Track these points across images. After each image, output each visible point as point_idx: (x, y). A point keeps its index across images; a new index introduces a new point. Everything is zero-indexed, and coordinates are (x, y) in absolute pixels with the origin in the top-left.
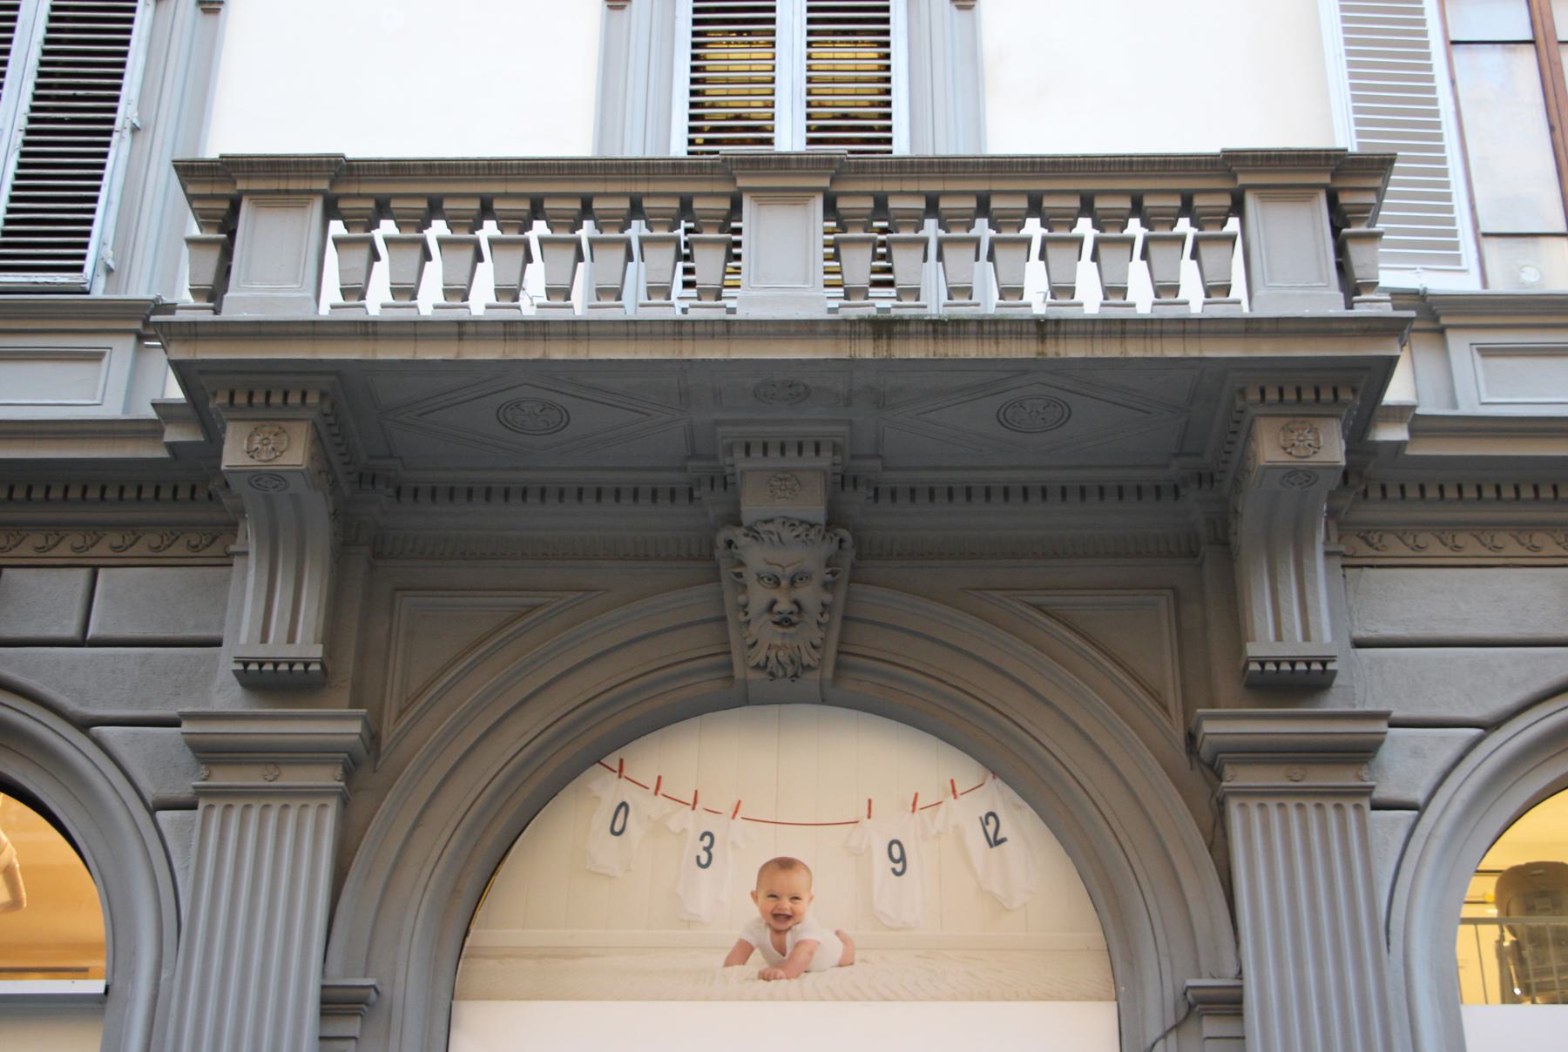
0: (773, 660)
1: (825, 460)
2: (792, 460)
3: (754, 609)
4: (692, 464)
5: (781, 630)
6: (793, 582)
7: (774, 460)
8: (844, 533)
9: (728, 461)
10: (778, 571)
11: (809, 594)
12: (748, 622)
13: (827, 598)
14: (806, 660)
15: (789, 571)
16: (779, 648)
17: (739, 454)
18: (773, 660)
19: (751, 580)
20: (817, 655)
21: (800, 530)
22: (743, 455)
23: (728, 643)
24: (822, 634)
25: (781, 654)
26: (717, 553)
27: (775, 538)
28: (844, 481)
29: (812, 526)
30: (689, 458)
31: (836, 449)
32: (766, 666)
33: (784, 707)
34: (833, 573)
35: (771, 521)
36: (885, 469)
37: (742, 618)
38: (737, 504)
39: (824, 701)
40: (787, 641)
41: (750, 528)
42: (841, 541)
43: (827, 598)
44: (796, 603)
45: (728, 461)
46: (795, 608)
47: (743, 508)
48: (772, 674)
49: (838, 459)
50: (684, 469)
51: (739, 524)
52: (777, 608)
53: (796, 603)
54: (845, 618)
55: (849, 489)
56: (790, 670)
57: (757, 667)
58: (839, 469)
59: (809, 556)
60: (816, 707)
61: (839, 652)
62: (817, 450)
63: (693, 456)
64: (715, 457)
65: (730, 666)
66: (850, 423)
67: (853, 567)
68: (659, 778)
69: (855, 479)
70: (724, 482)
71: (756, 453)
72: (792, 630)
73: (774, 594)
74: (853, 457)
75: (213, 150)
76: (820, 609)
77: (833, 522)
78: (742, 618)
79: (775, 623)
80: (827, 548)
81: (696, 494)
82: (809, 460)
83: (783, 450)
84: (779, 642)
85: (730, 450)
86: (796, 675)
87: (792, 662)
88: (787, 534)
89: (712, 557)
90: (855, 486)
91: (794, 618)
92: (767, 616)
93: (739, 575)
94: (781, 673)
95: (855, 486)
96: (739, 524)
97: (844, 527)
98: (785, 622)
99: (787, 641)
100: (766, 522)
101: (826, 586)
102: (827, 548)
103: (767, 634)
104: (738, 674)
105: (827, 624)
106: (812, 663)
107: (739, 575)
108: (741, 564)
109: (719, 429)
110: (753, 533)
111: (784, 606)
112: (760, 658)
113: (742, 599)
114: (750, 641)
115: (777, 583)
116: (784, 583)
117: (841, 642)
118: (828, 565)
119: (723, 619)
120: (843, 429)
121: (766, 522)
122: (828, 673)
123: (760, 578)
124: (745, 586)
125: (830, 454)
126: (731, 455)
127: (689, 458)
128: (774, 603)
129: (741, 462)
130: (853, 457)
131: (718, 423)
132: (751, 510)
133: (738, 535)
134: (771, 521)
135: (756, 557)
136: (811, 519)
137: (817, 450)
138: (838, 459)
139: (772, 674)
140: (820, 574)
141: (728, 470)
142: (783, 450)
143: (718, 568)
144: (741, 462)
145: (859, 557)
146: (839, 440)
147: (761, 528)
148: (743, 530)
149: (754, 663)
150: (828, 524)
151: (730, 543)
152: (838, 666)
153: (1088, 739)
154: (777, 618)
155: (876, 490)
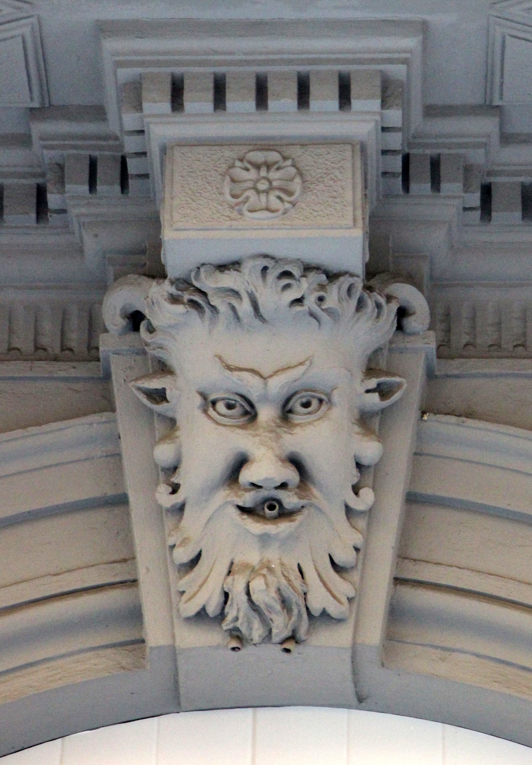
0: (238, 596)
1: (363, 120)
2: (283, 119)
3: (192, 479)
4: (39, 128)
5: (256, 527)
6: (286, 413)
7: (241, 120)
8: (407, 293)
9: (130, 120)
10: (252, 386)
11: (328, 441)
12: (181, 508)
13: (370, 450)
14: (319, 600)
15: (277, 386)
16: (254, 571)
17: (157, 104)
18: (238, 596)
19: (184, 403)
20: (343, 587)
21: (304, 286)
22: (166, 106)
23: (129, 559)
24: (358, 539)
25: (257, 584)
26: (107, 344)
27: (245, 307)
28: (409, 169)
29: (332, 276)
30: (34, 114)
31: (389, 92)
32: (221, 616)
33: (265, 715)
34: (383, 391)
35: (234, 265)
36: (506, 139)
37: (166, 499)
38: (155, 223)
39: (361, 700)
40: (273, 554)
41: (184, 283)
42: (402, 313)
43: (370, 450)
44: (296, 462)
45: (130, 120)
46: (291, 475)
47: (168, 235)
48: (236, 635)
49: (394, 116)
50: (24, 140)
51: (158, 273)
52: (247, 475)
53: (296, 462)
54: (412, 499)
55: (421, 186)
56: (281, 626)
57: (201, 615)
58: (395, 141)
59: (328, 349)
60: (341, 715)
61: (398, 581)
62: (345, 96)
63: (41, 112)
64: (98, 112)
65: (135, 615)
66: (424, 28)
67: (431, 375)
68: (299, 565)
69: (435, 164)
70: (121, 171)
71: (198, 102)
72: (283, 527)
73: (242, 440)
74: (431, 111)
75: (127, 159)
76: (354, 476)
77: (381, 269)
78: (166, 499)
79: (243, 510)
80: (368, 331)
81: (53, 200)
82: (324, 117)
83: (261, 94)
84: (253, 556)
85: (134, 94)
86: (293, 638)
87: (285, 603)
88: (273, 297)
89: (92, 353)
90: (436, 181)
91: (290, 500)
92: (223, 495)
93: (159, 396)
94: (257, 632)
95: (436, 181)
96: (158, 273)
97: (411, 279)
98: (268, 508)
99: (273, 554)
100: (222, 267)
101: (365, 420)
102: (368, 331)
103: (222, 533)
104: (155, 633)
105: (370, 513)
106: (334, 609)
107: (159, 396)
108: (164, 368)
109: (111, 45)
110: (192, 296)
111: (265, 469)
112: (209, 597)
113: (164, 453)
114: (183, 555)
115: (250, 413)
116: (267, 414)
117: (402, 556)
118: (370, 371)
119: (121, 501)
120: (410, 43)
121: (222, 267)
122: (373, 632)
123: (209, 403)
124: (172, 423)
125: (376, 104)
126: (139, 107)
127: (34, 114)
128: (241, 462)
129: (163, 126)
130: (431, 111)
131: (104, 29)
132: (190, 234)
133: (154, 298)
134: (234, 265)
135: (199, 352)
136: (334, 266)
137: (345, 96)
138: (394, 116)
139: (236, 635)
140: (352, 391)
141: (131, 145)
142: (261, 94)
143: (107, 377)
144: (163, 126)
145: (445, 350)
146: (398, 71)
147: (209, 282)
148: (167, 287)
149: (192, 608)
150: (372, 272)
151: (135, 319)
152: (396, 614)
153: (42, 45)
154: (248, 499)
155: (487, 192)
